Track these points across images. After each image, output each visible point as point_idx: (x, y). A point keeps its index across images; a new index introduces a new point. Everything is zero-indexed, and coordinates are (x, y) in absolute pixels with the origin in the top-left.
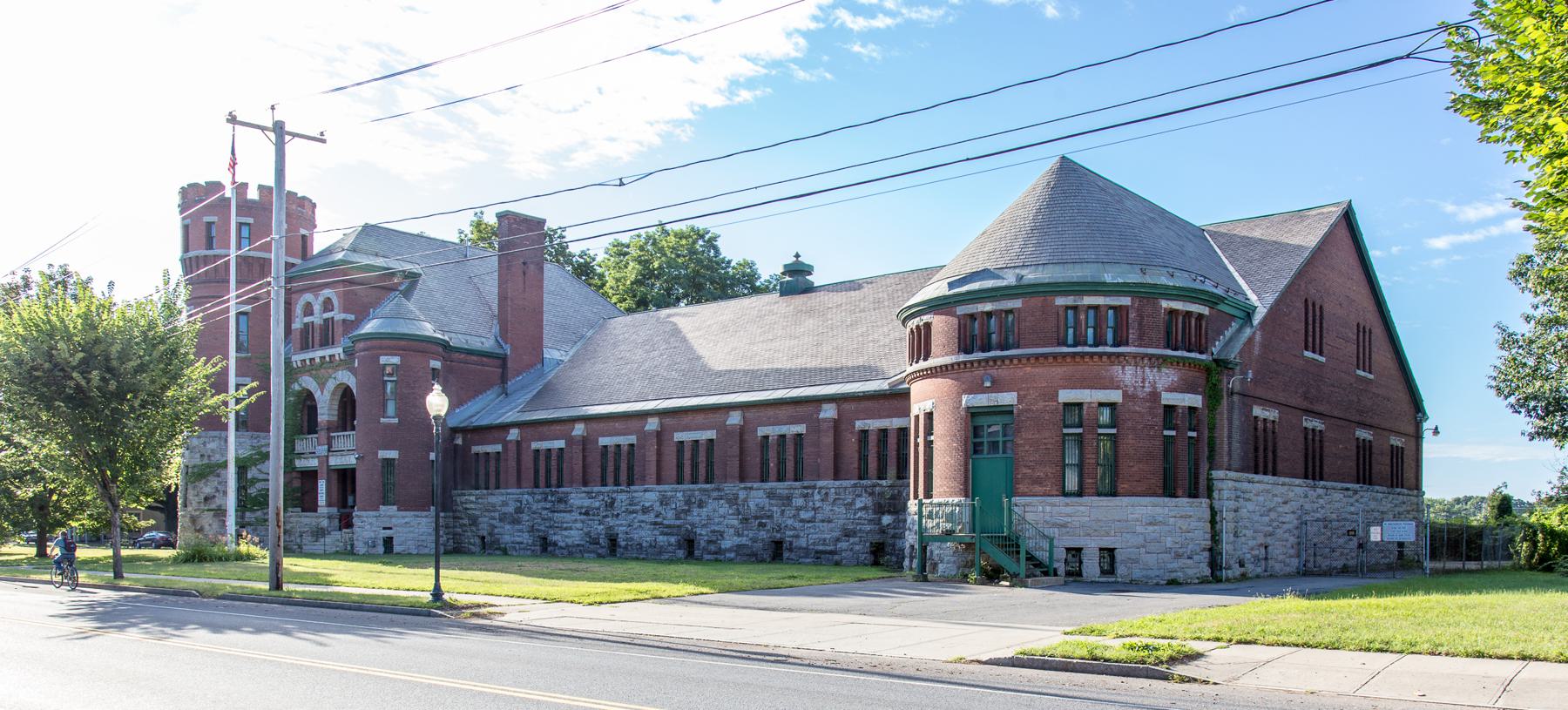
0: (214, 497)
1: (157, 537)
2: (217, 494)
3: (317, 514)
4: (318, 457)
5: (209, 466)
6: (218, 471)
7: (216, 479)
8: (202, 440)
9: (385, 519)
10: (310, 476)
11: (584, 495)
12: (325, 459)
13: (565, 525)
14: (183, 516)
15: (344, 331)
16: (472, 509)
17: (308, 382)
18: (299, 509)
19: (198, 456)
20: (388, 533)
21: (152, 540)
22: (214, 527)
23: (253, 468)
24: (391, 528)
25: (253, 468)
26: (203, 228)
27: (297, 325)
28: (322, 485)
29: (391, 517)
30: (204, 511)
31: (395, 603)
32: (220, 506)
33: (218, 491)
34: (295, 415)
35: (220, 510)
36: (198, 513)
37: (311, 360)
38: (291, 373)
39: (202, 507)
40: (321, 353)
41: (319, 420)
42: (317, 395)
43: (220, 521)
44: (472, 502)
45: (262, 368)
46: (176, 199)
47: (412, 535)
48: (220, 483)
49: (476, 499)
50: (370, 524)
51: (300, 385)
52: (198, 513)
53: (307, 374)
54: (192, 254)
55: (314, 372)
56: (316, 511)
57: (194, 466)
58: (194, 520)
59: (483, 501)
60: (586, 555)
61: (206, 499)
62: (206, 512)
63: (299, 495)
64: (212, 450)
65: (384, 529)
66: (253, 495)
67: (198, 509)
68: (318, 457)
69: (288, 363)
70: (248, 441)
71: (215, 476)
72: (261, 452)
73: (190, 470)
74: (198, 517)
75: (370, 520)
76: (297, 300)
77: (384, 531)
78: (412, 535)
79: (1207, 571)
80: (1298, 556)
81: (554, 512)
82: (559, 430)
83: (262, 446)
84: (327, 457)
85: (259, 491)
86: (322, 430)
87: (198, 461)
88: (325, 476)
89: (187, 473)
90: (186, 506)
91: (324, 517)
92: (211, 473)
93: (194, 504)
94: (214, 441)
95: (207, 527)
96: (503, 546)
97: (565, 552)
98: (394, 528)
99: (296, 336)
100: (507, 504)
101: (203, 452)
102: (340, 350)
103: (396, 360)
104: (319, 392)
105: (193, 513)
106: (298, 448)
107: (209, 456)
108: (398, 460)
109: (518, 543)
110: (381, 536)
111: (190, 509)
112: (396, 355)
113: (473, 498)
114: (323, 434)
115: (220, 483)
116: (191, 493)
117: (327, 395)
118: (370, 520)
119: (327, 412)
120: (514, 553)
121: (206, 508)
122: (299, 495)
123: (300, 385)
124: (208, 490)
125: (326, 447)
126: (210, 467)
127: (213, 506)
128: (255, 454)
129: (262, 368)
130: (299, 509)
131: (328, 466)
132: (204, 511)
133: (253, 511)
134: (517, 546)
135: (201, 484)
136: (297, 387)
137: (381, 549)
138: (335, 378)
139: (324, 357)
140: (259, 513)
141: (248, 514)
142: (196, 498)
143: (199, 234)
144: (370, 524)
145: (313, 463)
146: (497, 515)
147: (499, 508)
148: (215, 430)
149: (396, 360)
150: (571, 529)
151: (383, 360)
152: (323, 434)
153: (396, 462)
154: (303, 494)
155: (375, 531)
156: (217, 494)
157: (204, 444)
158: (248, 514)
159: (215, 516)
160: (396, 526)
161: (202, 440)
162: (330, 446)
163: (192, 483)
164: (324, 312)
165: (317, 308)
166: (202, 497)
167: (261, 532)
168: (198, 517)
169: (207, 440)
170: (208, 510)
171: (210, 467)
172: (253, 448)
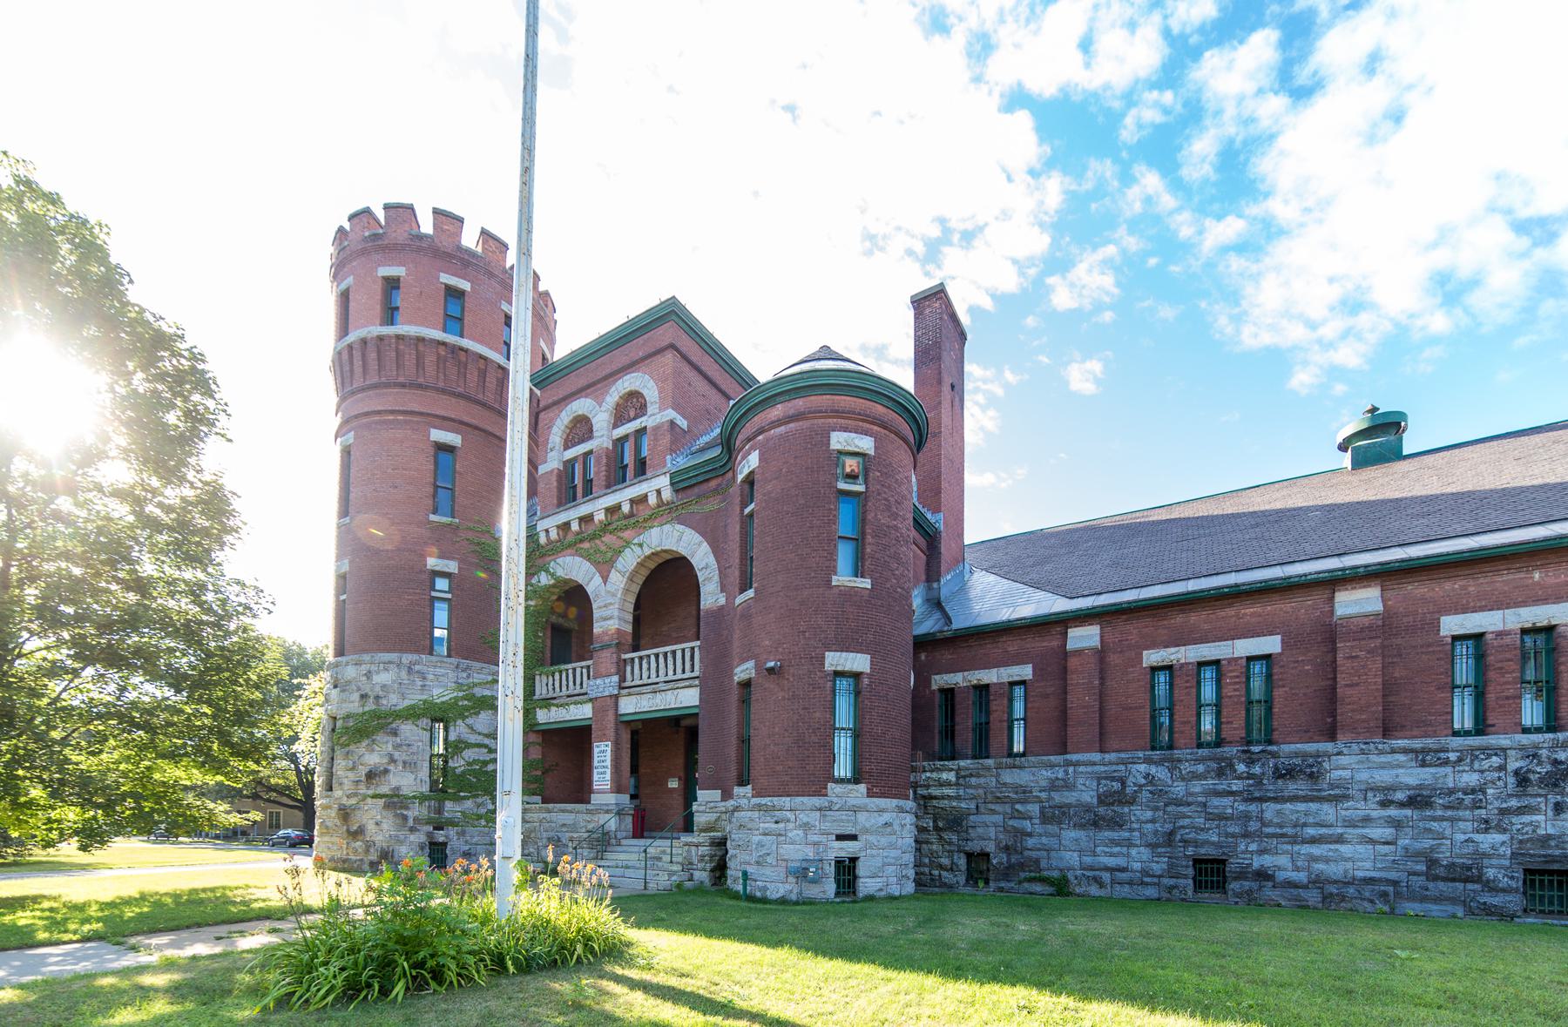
0: (386, 771)
1: (293, 835)
2: (391, 767)
3: (589, 807)
4: (591, 700)
5: (376, 715)
6: (394, 725)
7: (391, 739)
8: (364, 668)
9: (843, 815)
10: (575, 741)
11: (1402, 758)
12: (610, 702)
13: (1311, 831)
14: (325, 808)
15: (672, 443)
16: (949, 797)
17: (574, 568)
18: (538, 799)
19: (356, 696)
20: (849, 848)
21: (287, 838)
22: (385, 826)
23: (459, 722)
24: (853, 838)
25: (459, 722)
26: (378, 288)
27: (552, 463)
28: (603, 754)
29: (855, 810)
30: (365, 797)
31: (687, 968)
32: (398, 788)
33: (393, 760)
34: (536, 636)
35: (398, 796)
36: (353, 801)
37: (582, 520)
38: (537, 555)
39: (363, 790)
40: (609, 500)
41: (596, 630)
42: (593, 585)
43: (396, 815)
44: (948, 784)
45: (477, 548)
46: (324, 253)
47: (894, 853)
48: (397, 747)
49: (958, 778)
50: (806, 827)
51: (553, 575)
52: (353, 801)
53: (569, 551)
54: (352, 337)
55: (586, 545)
56: (585, 800)
57: (348, 717)
58: (345, 814)
59: (982, 780)
60: (1411, 908)
61: (371, 776)
62: (369, 800)
63: (539, 773)
64: (384, 687)
65: (840, 838)
66: (458, 771)
67: (355, 795)
68: (591, 700)
69: (532, 536)
70: (451, 675)
71: (388, 734)
72: (474, 695)
73: (339, 724)
74: (355, 808)
75: (803, 817)
76: (552, 421)
77: (838, 844)
78: (894, 853)
79: (702, 876)
80: (1309, 882)
81: (1261, 800)
82: (1252, 615)
83: (475, 685)
84: (616, 697)
85: (469, 764)
86: (602, 648)
87: (354, 706)
88: (611, 733)
89: (333, 730)
90: (331, 789)
91: (607, 812)
92: (381, 727)
93: (348, 785)
94: (386, 670)
95: (371, 827)
96: (1056, 874)
97: (1313, 897)
98: (862, 838)
99: (549, 488)
100: (1068, 786)
101: (367, 689)
102: (663, 482)
103: (866, 444)
104: (598, 579)
105: (345, 801)
106: (541, 690)
107: (377, 698)
108: (870, 676)
109: (1107, 869)
110: (832, 855)
111: (337, 793)
112: (866, 433)
113: (951, 776)
114: (606, 659)
115: (397, 747)
116: (341, 764)
117: (618, 580)
118: (803, 817)
119: (616, 613)
120: (1094, 890)
121: (370, 792)
122: (539, 773)
123: (553, 575)
124: (374, 759)
125: (616, 679)
126: (379, 718)
127: (384, 789)
128: (463, 698)
129: (477, 548)
130: (538, 799)
131: (617, 715)
132: (365, 797)
133: (457, 799)
134: (1106, 876)
135: (361, 748)
136: (544, 580)
137: (830, 888)
138: (641, 545)
139: (618, 507)
140: (469, 804)
141: (449, 805)
142: (350, 774)
143: (369, 301)
144: (806, 827)
145: (583, 712)
146: (1034, 809)
147: (1043, 795)
148: (389, 651)
149: (866, 444)
150: (1340, 840)
151: (839, 440)
152: (606, 659)
153: (866, 681)
154: (543, 773)
155: (815, 844)
156: (391, 767)
157: (369, 675)
158: (449, 805)
159: (387, 806)
160: (866, 831)
161: (364, 668)
162: (623, 679)
163: (343, 746)
164: (614, 428)
165: (601, 420)
166: (363, 771)
167: (472, 837)
168: (355, 808)
169: (374, 668)
170: (374, 796)
171: (379, 718)
172: (459, 686)
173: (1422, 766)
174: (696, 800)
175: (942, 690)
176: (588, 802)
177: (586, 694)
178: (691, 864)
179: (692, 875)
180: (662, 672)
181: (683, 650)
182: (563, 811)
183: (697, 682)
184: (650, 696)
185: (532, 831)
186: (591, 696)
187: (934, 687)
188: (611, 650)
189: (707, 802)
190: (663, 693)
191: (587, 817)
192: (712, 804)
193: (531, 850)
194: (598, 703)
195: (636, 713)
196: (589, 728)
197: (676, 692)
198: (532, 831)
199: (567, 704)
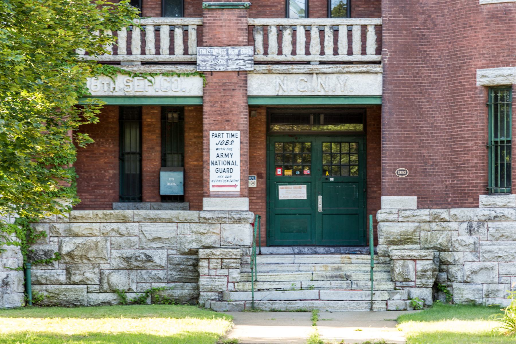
4: (201, 74)
68: (201, 74)
173: (414, 309)
174: (380, 209)
175: (491, 89)
176: (200, 208)
177: (194, 63)
178: (407, 280)
179: (409, 294)
180: (315, 48)
181: (364, 28)
182: (153, 220)
183: (378, 68)
184: (305, 77)
185: (90, 249)
186: (202, 69)
187: (478, 84)
188: (237, 12)
189: (399, 210)
190: (323, 76)
191: (202, 228)
192: (408, 213)
193: (88, 275)
194: (213, 80)
195: (278, 97)
196: (199, 109)
197: (343, 77)
198: (90, 249)
199: (151, 74)
